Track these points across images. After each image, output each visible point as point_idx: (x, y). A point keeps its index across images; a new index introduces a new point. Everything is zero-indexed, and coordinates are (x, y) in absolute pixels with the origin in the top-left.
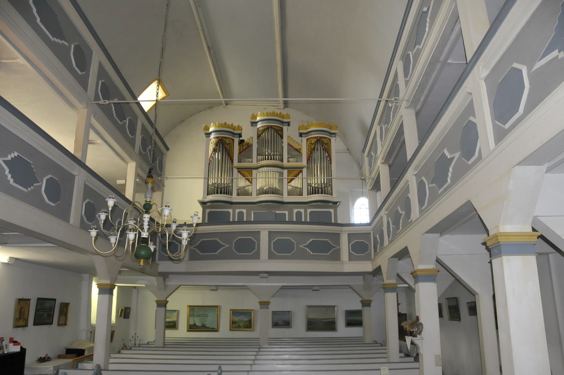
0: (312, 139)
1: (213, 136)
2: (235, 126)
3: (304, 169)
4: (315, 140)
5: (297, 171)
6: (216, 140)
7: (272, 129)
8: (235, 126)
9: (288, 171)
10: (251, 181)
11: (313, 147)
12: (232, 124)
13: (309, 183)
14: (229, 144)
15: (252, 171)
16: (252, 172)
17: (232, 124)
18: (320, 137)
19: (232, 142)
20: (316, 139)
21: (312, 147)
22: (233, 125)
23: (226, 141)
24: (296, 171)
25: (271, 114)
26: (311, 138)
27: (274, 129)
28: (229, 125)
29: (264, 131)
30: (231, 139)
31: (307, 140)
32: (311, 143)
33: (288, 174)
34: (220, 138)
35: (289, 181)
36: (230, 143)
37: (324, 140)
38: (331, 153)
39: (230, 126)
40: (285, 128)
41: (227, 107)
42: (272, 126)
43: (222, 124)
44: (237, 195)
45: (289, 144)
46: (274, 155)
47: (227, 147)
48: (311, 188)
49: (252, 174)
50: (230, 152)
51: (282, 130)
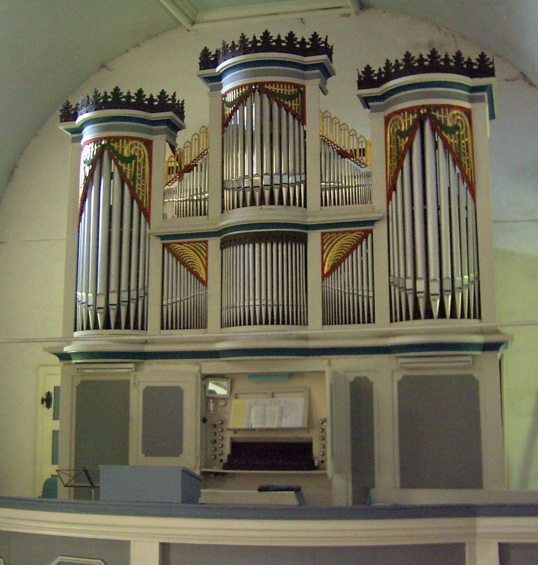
0: (400, 118)
1: (88, 134)
2: (469, 59)
3: (376, 225)
4: (411, 118)
5: (349, 236)
6: (96, 148)
7: (265, 96)
8: (469, 59)
9: (323, 234)
10: (203, 276)
11: (405, 146)
12: (140, 93)
13: (396, 275)
14: (456, 128)
15: (206, 242)
16: (207, 247)
17: (140, 93)
18: (428, 107)
19: (467, 120)
20: (416, 116)
21: (403, 143)
22: (463, 59)
23: (445, 119)
24: (351, 232)
25: (237, 49)
26: (398, 113)
27: (272, 96)
28: (421, 60)
29: (240, 102)
30: (139, 143)
31: (387, 119)
32: (399, 133)
33: (323, 244)
34: (103, 143)
35: (327, 273)
36: (137, 154)
37: (435, 114)
38: (472, 162)
39: (452, 64)
40: (312, 87)
41: (195, 30)
42: (262, 84)
43: (106, 96)
44: (162, 328)
45: (325, 141)
46: (281, 184)
47: (452, 140)
48: (403, 294)
49: (206, 252)
50: (463, 158)
51: (300, 93)
